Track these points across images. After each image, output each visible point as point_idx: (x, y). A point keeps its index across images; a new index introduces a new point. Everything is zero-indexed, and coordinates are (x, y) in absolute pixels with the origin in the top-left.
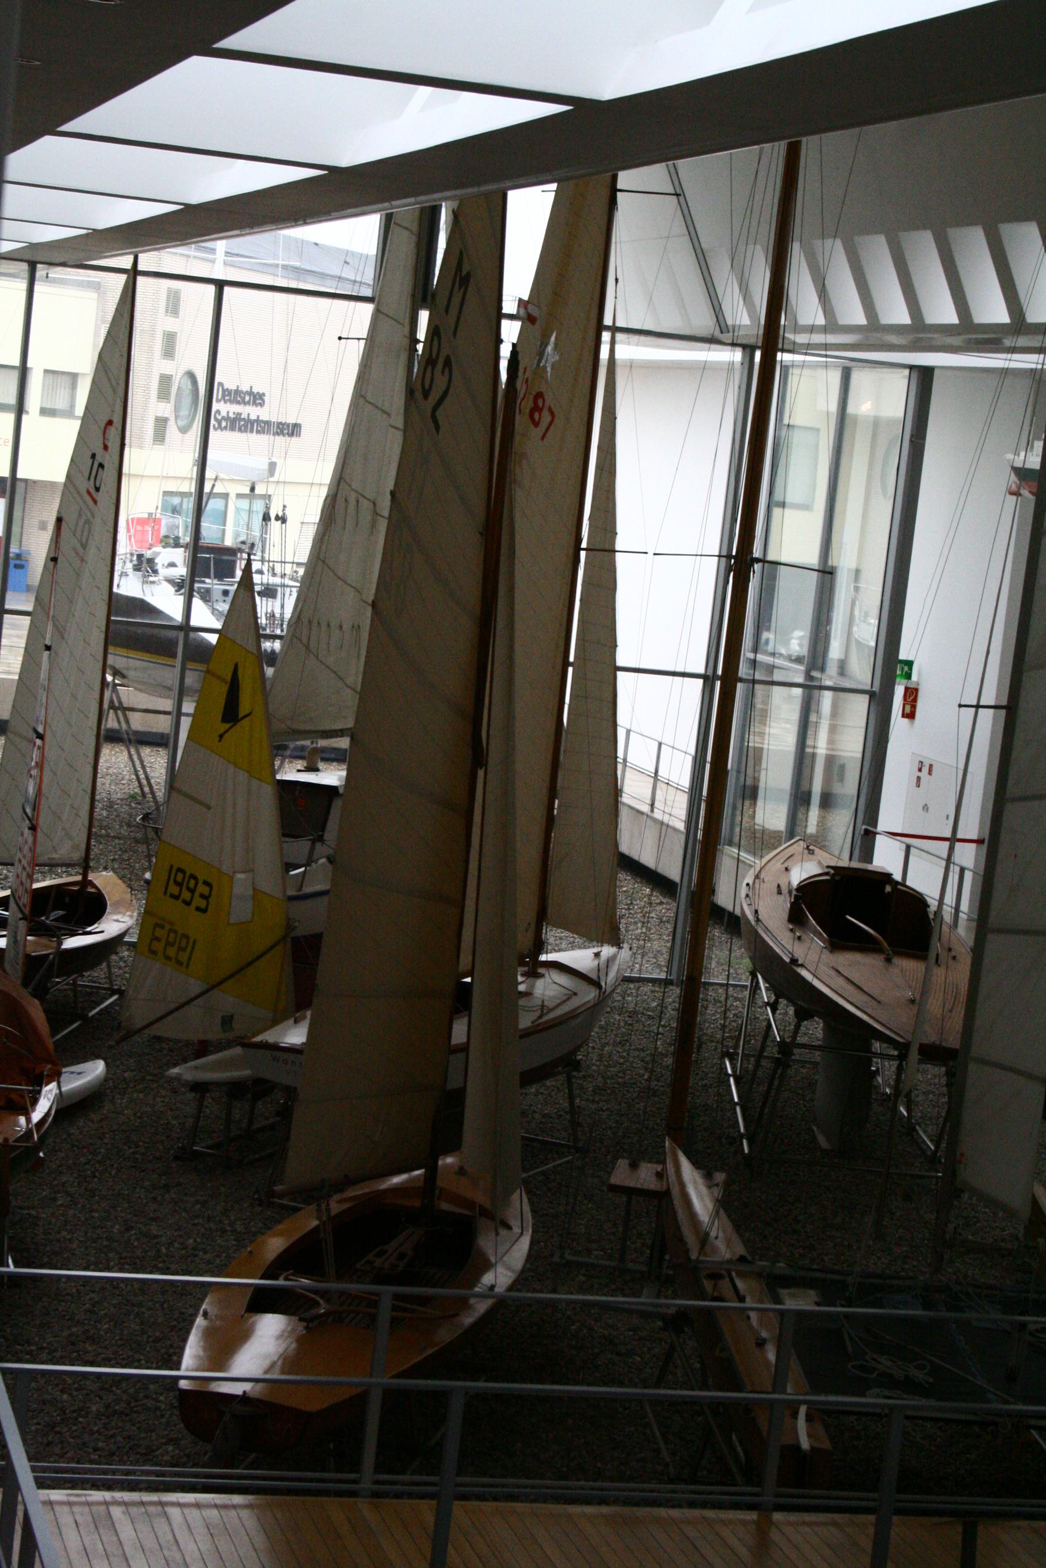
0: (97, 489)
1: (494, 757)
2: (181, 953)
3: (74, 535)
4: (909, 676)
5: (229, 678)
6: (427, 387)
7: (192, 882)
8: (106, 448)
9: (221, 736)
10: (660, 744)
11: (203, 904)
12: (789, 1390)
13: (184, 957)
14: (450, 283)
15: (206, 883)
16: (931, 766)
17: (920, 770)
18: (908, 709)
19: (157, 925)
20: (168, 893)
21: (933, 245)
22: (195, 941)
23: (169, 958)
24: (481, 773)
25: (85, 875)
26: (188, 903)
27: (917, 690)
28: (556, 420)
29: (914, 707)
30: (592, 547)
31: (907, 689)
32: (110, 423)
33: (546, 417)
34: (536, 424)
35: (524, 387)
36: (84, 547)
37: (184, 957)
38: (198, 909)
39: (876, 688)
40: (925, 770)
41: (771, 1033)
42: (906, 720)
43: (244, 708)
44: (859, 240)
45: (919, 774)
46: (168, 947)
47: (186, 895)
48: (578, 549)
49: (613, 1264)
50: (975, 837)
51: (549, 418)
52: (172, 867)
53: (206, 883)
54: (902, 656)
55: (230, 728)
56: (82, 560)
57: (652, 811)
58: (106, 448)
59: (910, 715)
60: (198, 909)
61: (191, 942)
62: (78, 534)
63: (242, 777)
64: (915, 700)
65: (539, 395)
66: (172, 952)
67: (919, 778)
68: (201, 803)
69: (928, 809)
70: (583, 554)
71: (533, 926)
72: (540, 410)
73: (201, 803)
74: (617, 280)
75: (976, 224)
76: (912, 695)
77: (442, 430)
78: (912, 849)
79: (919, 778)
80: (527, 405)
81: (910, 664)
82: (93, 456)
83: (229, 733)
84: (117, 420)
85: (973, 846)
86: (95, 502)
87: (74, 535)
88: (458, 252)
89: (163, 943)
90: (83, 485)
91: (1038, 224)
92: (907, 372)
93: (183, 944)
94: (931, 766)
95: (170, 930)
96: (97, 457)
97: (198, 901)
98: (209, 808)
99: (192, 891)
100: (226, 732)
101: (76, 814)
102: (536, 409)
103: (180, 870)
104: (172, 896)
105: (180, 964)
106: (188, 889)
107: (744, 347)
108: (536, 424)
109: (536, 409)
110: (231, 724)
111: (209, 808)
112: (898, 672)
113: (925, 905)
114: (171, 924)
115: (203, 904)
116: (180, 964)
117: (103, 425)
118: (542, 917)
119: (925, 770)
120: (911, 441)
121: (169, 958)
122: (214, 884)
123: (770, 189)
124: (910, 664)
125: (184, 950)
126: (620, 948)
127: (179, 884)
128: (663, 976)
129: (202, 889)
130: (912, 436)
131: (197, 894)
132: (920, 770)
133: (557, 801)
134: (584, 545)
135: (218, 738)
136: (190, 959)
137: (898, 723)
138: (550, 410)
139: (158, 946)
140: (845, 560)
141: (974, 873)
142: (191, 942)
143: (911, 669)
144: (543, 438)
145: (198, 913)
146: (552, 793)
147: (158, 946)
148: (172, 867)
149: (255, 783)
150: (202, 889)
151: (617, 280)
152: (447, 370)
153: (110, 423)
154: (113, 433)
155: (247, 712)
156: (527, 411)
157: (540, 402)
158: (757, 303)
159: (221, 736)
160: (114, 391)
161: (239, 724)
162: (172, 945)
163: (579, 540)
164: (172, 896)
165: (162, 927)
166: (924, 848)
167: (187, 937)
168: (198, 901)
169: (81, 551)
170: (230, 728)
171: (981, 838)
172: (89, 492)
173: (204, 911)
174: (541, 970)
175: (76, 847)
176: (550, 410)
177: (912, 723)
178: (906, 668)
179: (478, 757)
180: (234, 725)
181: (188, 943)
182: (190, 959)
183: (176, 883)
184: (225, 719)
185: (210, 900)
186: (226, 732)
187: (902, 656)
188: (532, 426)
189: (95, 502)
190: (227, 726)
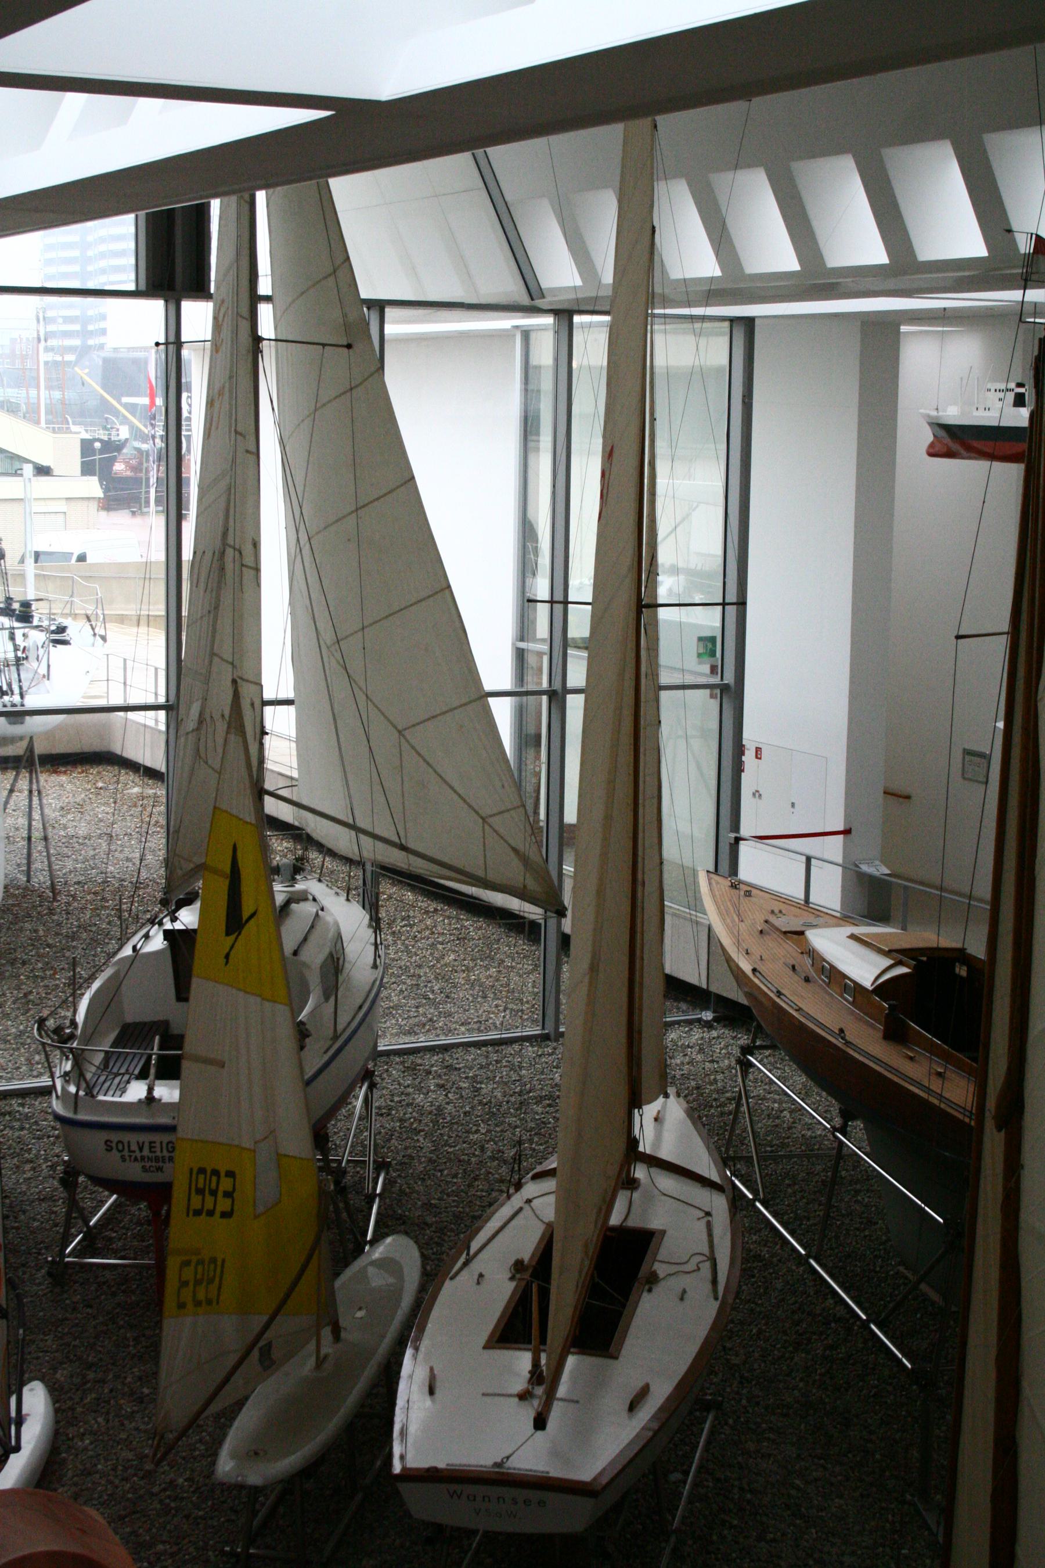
5: (228, 869)
9: (227, 957)
10: (809, 860)
21: (767, 182)
41: (845, 1151)
44: (721, 181)
50: (841, 828)
55: (236, 938)
61: (219, 1263)
69: (760, 795)
75: (943, 138)
78: (813, 861)
85: (840, 838)
91: (854, 156)
92: (727, 324)
97: (224, 1204)
98: (222, 1065)
103: (202, 1171)
105: (209, 1302)
107: (556, 312)
110: (236, 934)
111: (222, 1065)
128: (536, 1031)
129: (226, 1184)
141: (844, 867)
142: (219, 1263)
148: (191, 1170)
150: (226, 1184)
155: (252, 911)
158: (598, 261)
166: (787, 847)
168: (224, 1204)
170: (236, 938)
171: (848, 828)
174: (640, 1172)
180: (239, 934)
185: (235, 1195)
190: (233, 937)
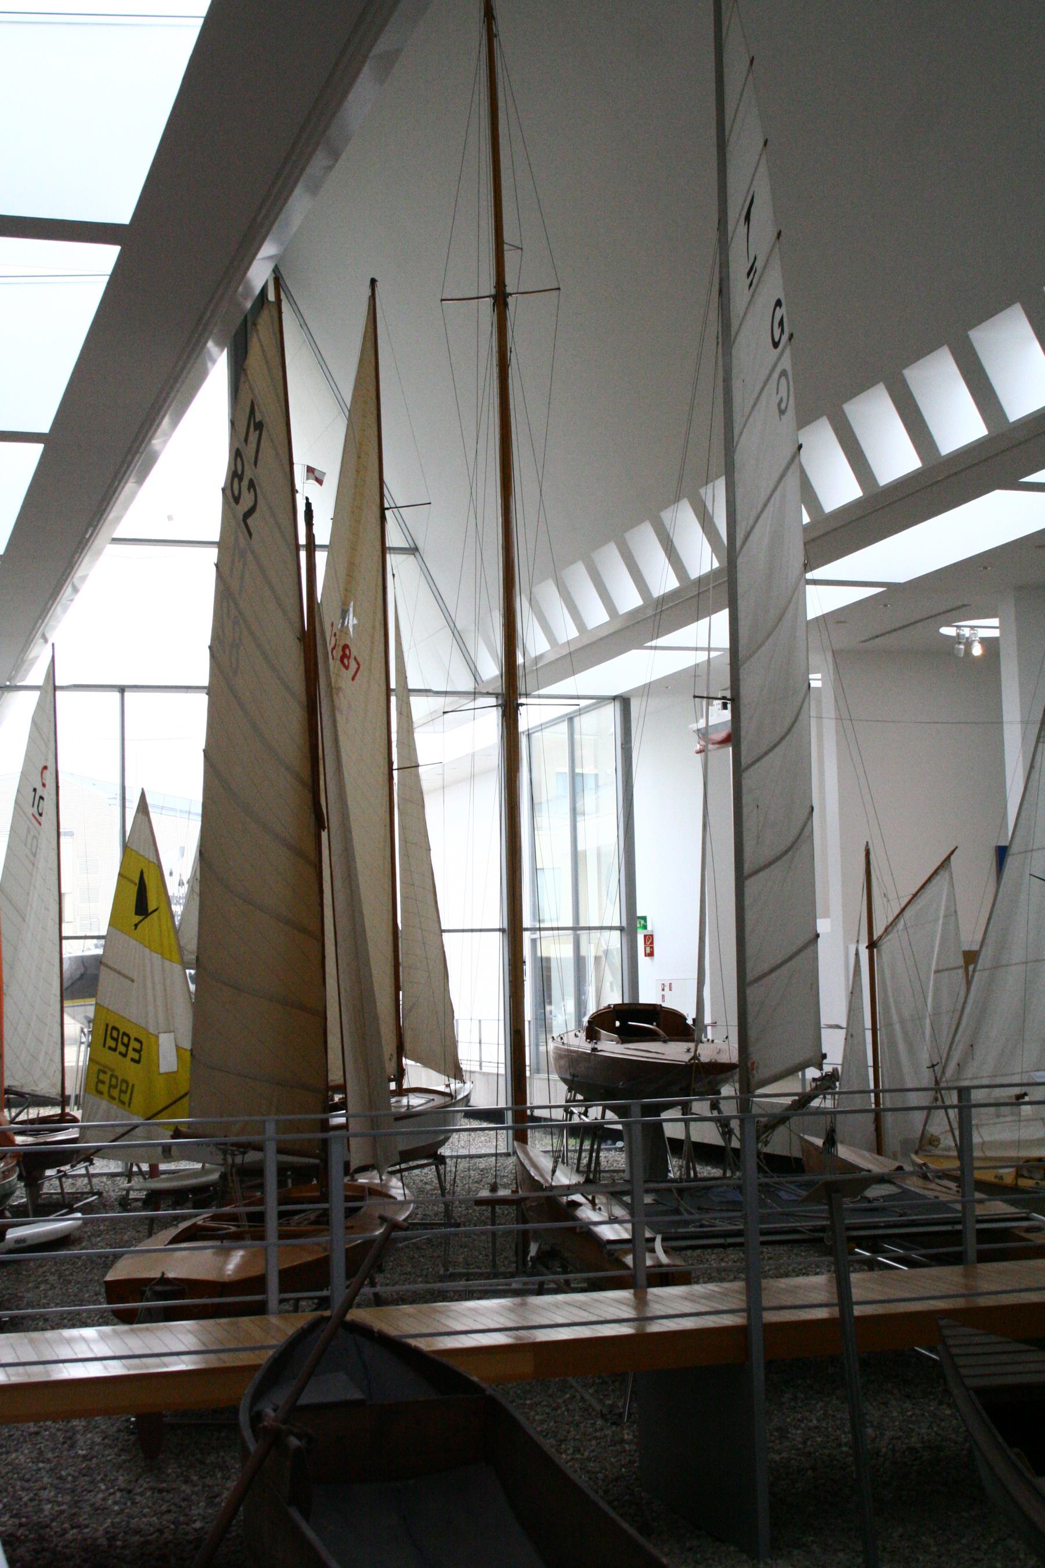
0: (41, 815)
1: (334, 820)
2: (122, 1095)
3: (25, 844)
4: (645, 927)
5: (137, 881)
6: (236, 493)
7: (126, 1040)
8: (44, 785)
9: (136, 926)
11: (136, 1056)
12: (639, 1127)
13: (126, 1098)
14: (246, 422)
15: (136, 1039)
16: (670, 985)
17: (663, 990)
18: (648, 950)
19: (100, 1071)
20: (107, 1046)
22: (133, 1086)
23: (113, 1098)
24: (324, 835)
25: (63, 1109)
26: (125, 1055)
27: (652, 936)
28: (361, 667)
29: (652, 948)
30: (402, 766)
31: (645, 936)
32: (45, 768)
33: (353, 666)
34: (347, 668)
35: (333, 639)
36: (35, 855)
37: (126, 1098)
38: (133, 1060)
39: (624, 924)
40: (667, 988)
42: (647, 958)
43: (151, 907)
45: (663, 993)
46: (112, 1090)
47: (121, 1048)
48: (391, 770)
49: (488, 1270)
51: (356, 666)
52: (107, 1025)
53: (136, 1039)
54: (639, 914)
56: (33, 864)
57: (481, 1069)
58: (44, 785)
59: (651, 954)
60: (133, 1060)
62: (29, 846)
63: (156, 957)
64: (652, 943)
65: (346, 647)
66: (115, 1093)
67: (663, 996)
68: (126, 977)
70: (395, 773)
71: (395, 1056)
72: (349, 658)
73: (126, 977)
74: (394, 575)
76: (649, 939)
77: (254, 536)
79: (663, 996)
80: (338, 653)
81: (644, 918)
82: (35, 790)
83: (143, 922)
84: (51, 765)
86: (40, 824)
87: (25, 844)
88: (249, 404)
89: (107, 1085)
90: (31, 811)
93: (124, 1088)
94: (670, 985)
95: (112, 1076)
96: (38, 791)
97: (132, 1054)
98: (133, 981)
99: (127, 1046)
100: (140, 922)
101: (51, 1060)
102: (344, 657)
104: (110, 1048)
105: (123, 1103)
106: (123, 1044)
108: (347, 668)
109: (344, 657)
112: (638, 925)
113: (682, 1018)
114: (113, 1070)
115: (136, 1056)
116: (123, 1103)
117: (40, 769)
118: (401, 1051)
119: (667, 988)
120: (622, 748)
121: (113, 1098)
122: (144, 1041)
123: (491, 436)
124: (644, 918)
125: (125, 1092)
126: (464, 1083)
127: (116, 1040)
129: (134, 1044)
130: (622, 744)
131: (130, 1048)
132: (663, 990)
133: (401, 992)
134: (395, 766)
135: (134, 927)
136: (130, 1099)
137: (642, 959)
138: (355, 659)
139: (104, 1088)
140: (586, 768)
142: (130, 1085)
143: (646, 922)
144: (353, 679)
145: (132, 1063)
146: (397, 988)
147: (104, 1088)
149: (167, 963)
150: (134, 1044)
151: (394, 575)
152: (252, 490)
153: (45, 768)
154: (49, 776)
155: (154, 908)
156: (339, 658)
157: (347, 652)
159: (136, 926)
160: (47, 746)
161: (149, 917)
162: (115, 1087)
163: (390, 763)
164: (110, 1048)
165: (105, 1073)
167: (127, 1083)
169: (31, 857)
172: (34, 816)
173: (138, 1062)
175: (54, 1085)
176: (355, 659)
177: (653, 960)
178: (642, 922)
179: (320, 822)
181: (127, 1088)
182: (130, 1099)
183: (113, 1038)
184: (137, 913)
185: (142, 1053)
186: (140, 922)
187: (639, 914)
188: (343, 669)
189: (40, 824)
190: (141, 918)
